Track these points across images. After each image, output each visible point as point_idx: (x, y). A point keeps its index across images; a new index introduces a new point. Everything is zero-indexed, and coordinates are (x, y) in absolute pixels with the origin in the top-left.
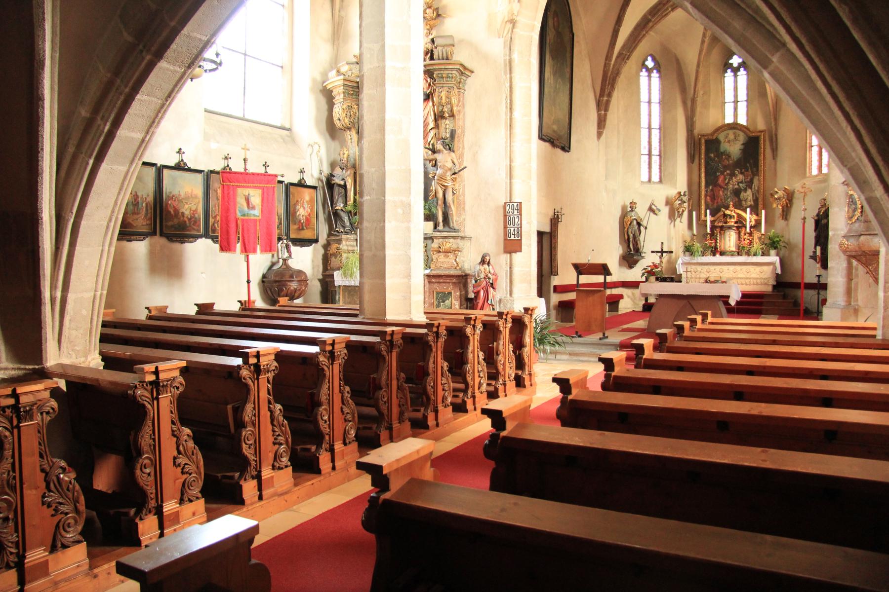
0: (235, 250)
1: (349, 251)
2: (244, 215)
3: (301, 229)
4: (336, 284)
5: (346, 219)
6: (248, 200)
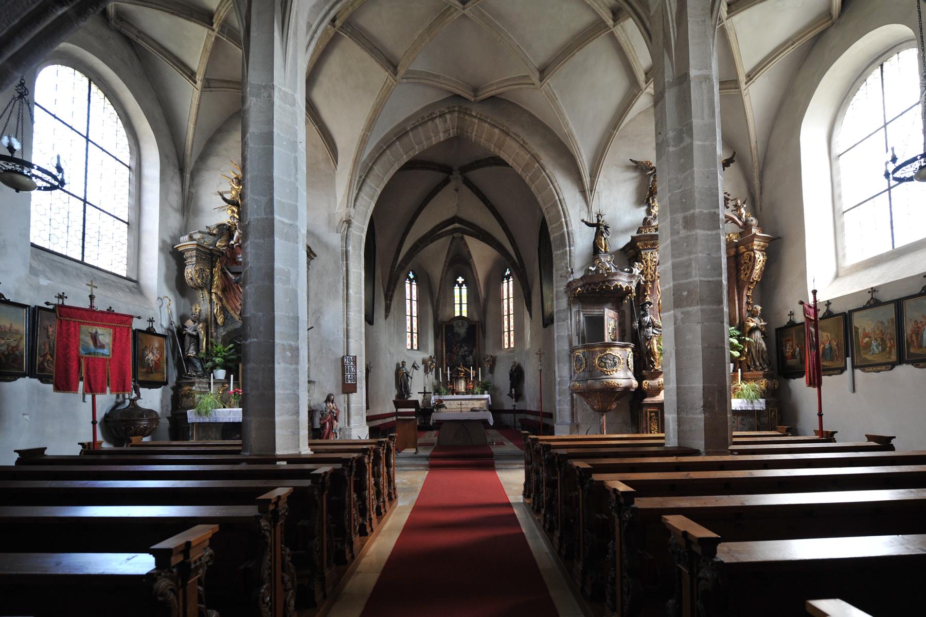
0: (75, 390)
1: (201, 393)
2: (90, 353)
3: (150, 371)
4: (189, 421)
5: (198, 365)
6: (94, 338)
